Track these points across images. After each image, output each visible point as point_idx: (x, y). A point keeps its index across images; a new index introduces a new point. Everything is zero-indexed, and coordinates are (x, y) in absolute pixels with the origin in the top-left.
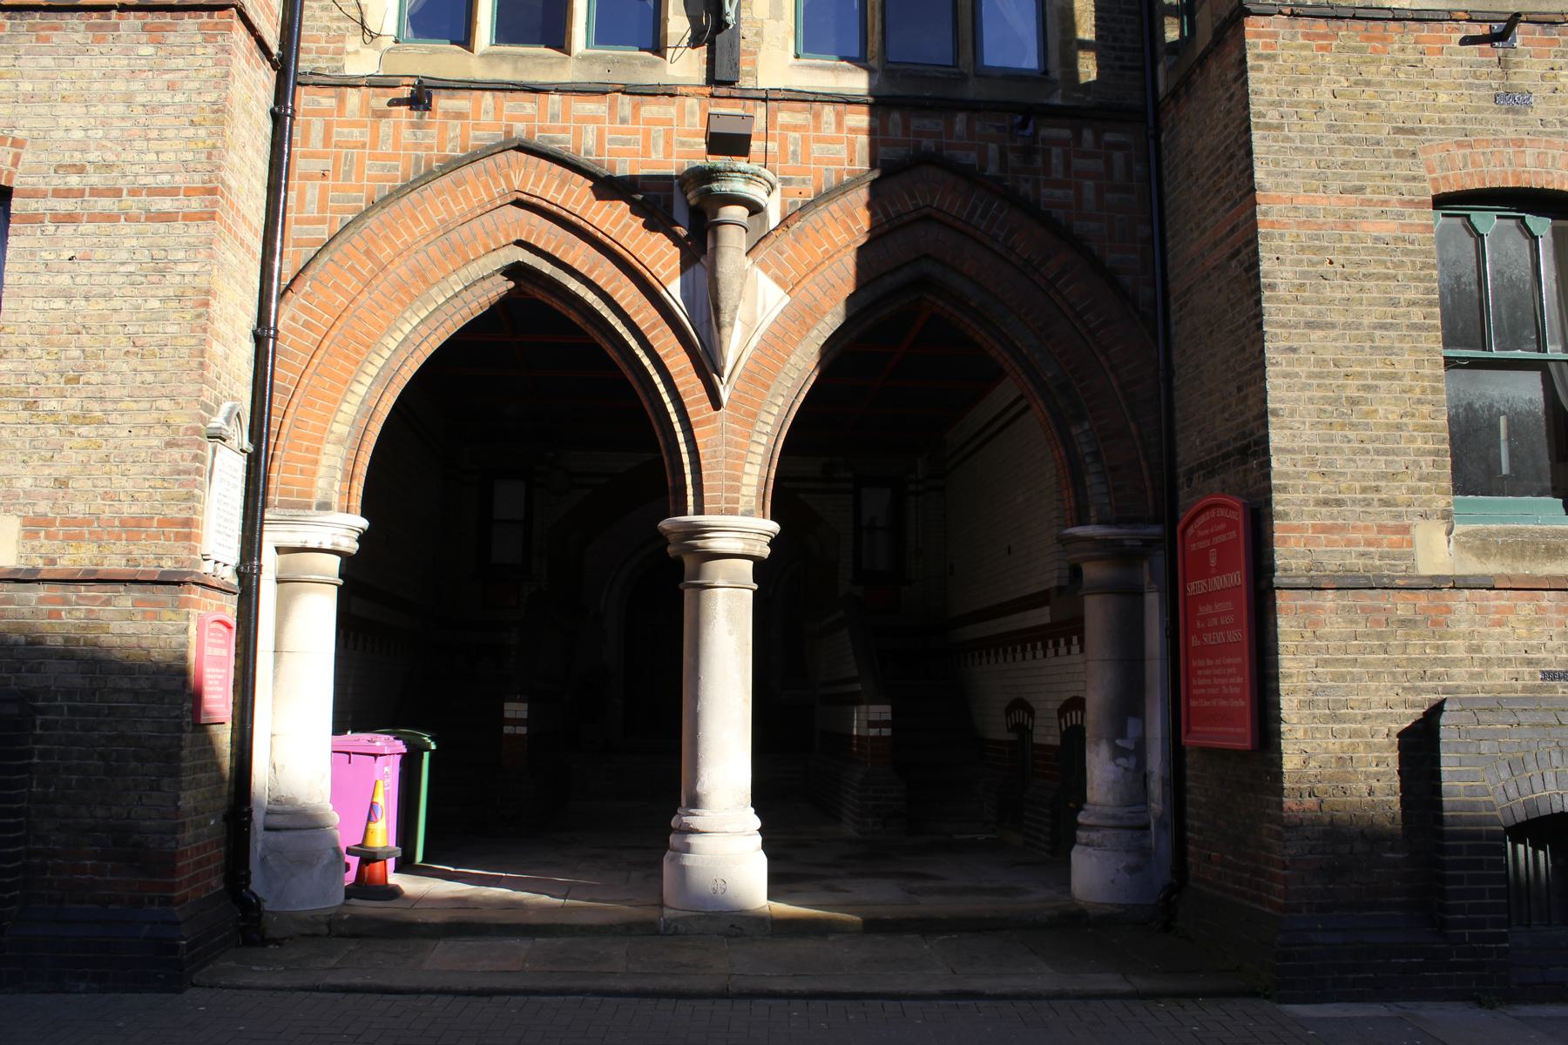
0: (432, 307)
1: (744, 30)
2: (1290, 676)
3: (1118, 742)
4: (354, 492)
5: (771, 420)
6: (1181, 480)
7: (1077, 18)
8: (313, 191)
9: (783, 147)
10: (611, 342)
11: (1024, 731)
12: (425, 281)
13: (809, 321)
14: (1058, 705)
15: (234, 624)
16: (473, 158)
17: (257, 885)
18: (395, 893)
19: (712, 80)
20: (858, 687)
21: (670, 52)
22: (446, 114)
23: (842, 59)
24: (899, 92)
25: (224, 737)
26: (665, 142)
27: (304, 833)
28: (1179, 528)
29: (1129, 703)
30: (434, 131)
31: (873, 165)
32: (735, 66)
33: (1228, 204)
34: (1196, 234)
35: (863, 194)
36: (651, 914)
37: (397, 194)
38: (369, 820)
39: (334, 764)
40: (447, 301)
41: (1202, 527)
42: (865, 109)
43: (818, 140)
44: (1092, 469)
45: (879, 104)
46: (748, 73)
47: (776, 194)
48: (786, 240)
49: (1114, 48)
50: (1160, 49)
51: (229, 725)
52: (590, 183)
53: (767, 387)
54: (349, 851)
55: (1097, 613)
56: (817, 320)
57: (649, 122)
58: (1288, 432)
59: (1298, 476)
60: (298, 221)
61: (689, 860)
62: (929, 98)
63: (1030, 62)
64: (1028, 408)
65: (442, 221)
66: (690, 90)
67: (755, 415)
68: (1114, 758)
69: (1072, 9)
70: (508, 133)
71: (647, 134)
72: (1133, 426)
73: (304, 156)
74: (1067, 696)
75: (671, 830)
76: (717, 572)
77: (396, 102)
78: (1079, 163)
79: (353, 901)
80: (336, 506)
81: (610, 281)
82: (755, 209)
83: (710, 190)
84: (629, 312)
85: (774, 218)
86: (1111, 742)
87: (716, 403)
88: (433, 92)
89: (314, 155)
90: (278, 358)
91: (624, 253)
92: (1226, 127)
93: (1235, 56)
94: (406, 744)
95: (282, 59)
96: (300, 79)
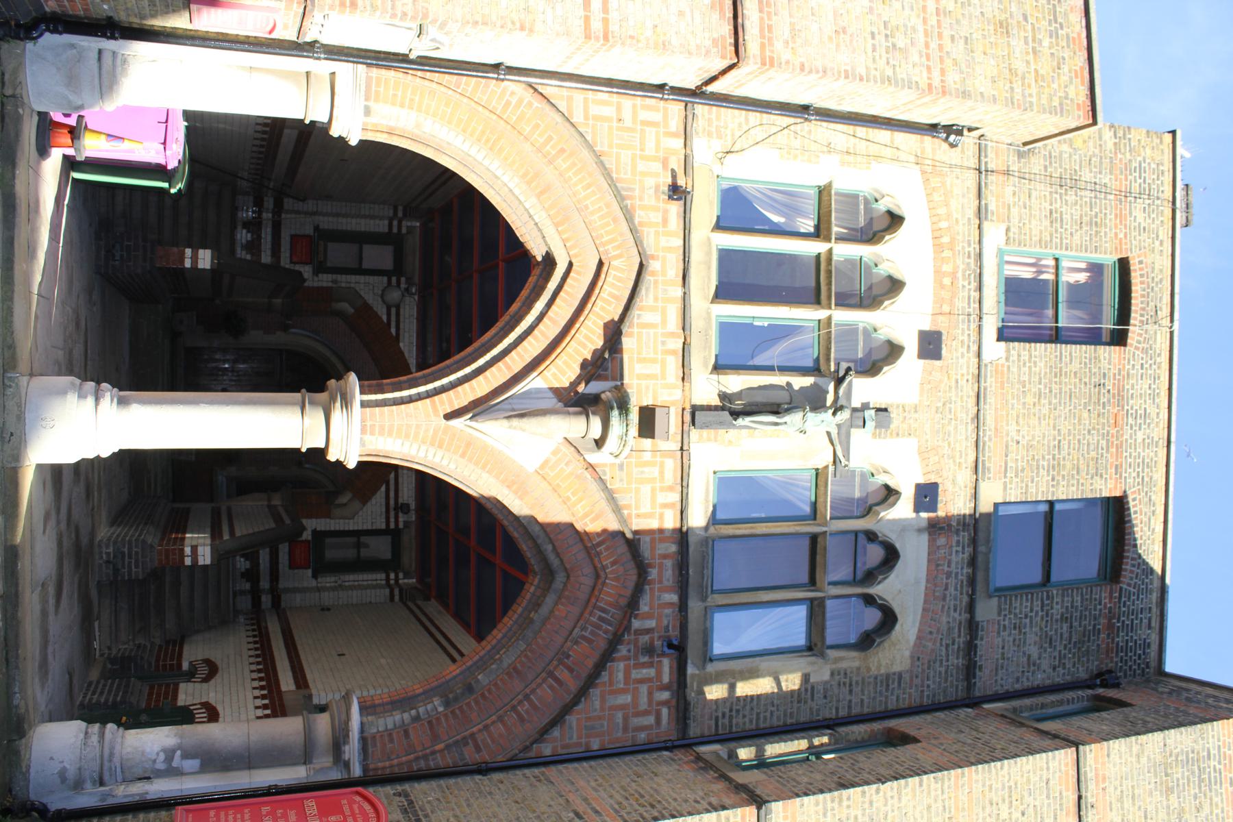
0: (522, 198)
1: (732, 432)
3: (179, 753)
4: (379, 135)
5: (437, 460)
6: (399, 788)
7: (752, 681)
8: (609, 111)
9: (646, 464)
10: (496, 334)
11: (190, 675)
12: (542, 193)
13: (515, 487)
14: (213, 702)
15: (273, 36)
16: (633, 230)
17: (49, 39)
18: (43, 152)
19: (695, 409)
20: (226, 537)
21: (715, 377)
22: (666, 212)
23: (715, 507)
24: (691, 549)
25: (179, 22)
26: (648, 374)
27: (97, 81)
28: (360, 789)
29: (214, 760)
30: (653, 202)
31: (636, 533)
32: (706, 426)
33: (617, 807)
34: (593, 784)
35: (614, 526)
36: (23, 365)
37: (607, 174)
38: (109, 135)
39: (157, 110)
40: (526, 210)
41: (361, 807)
42: (678, 525)
43: (653, 490)
44: (406, 716)
45: (682, 536)
46: (701, 436)
47: (612, 460)
48: (577, 467)
49: (731, 710)
50: (732, 745)
51: (190, 27)
52: (616, 319)
53: (463, 455)
54: (81, 117)
55: (288, 728)
56: (516, 493)
57: (663, 363)
60: (586, 100)
61: (72, 398)
62: (687, 573)
63: (718, 648)
64: (454, 660)
65: (587, 207)
66: (687, 393)
67: (440, 447)
68: (164, 750)
69: (758, 677)
70: (653, 257)
71: (654, 361)
72: (442, 746)
73: (634, 106)
74: (220, 709)
75: (98, 383)
76: (315, 418)
77: (674, 176)
78: (644, 689)
79: (36, 118)
80: (368, 120)
81: (543, 334)
82: (599, 443)
83: (612, 408)
84: (519, 348)
85: (594, 457)
86: (180, 747)
87: (448, 417)
88: (682, 202)
89: (635, 113)
90: (484, 81)
91: (563, 345)
92: (675, 800)
93: (727, 801)
94: (175, 170)
95: (703, 93)
96: (689, 105)
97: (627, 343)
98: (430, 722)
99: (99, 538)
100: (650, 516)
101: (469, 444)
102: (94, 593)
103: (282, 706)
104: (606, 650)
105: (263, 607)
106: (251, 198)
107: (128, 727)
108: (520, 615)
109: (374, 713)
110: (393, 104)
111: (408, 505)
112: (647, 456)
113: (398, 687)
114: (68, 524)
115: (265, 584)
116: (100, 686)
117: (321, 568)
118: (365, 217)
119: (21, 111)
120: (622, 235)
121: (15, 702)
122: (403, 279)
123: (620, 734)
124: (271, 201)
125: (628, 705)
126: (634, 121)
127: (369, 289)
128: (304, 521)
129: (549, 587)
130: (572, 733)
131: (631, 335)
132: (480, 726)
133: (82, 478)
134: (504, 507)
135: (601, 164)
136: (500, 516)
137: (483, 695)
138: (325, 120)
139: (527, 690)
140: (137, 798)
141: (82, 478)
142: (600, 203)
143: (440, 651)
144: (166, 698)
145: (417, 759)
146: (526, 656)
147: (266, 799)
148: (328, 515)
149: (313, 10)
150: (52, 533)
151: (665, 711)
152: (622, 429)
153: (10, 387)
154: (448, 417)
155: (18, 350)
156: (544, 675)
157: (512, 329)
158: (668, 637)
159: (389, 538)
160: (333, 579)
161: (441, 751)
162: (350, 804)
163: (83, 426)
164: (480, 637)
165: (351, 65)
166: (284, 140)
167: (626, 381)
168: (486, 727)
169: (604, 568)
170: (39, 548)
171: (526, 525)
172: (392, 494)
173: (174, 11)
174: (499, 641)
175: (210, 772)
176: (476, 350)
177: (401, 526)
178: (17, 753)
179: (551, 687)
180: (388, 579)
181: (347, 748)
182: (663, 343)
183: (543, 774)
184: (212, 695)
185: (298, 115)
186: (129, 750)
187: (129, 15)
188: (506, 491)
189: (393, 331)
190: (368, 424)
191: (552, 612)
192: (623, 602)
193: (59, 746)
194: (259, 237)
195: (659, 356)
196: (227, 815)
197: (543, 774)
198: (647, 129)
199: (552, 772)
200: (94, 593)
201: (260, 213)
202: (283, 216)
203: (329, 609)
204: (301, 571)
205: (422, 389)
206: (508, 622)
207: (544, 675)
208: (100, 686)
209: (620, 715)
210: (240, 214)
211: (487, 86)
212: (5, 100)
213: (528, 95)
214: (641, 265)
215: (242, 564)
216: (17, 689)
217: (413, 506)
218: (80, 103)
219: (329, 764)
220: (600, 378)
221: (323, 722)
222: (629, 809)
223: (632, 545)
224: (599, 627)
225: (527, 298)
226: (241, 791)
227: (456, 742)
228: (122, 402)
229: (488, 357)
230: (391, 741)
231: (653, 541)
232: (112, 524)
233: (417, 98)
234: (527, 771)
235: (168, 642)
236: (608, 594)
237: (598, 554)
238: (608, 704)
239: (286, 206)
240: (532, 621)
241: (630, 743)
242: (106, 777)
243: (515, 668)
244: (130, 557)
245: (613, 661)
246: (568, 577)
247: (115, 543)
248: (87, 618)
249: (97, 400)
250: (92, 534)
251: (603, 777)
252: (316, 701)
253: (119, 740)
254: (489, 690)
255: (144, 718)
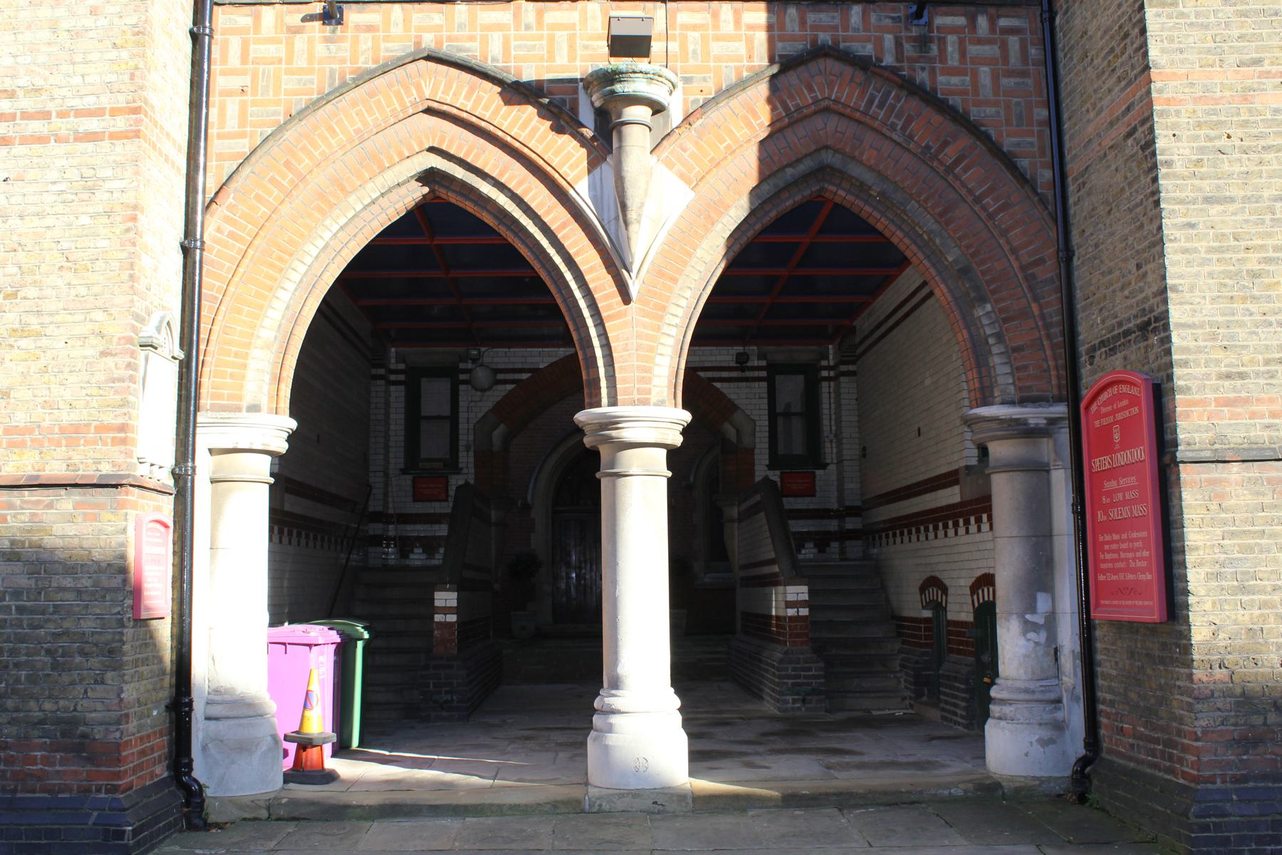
0: (350, 214)
2: (1197, 548)
3: (1028, 617)
4: (282, 394)
5: (680, 312)
6: (1084, 358)
8: (232, 106)
9: (683, 46)
10: (523, 242)
11: (939, 608)
12: (343, 189)
13: (713, 215)
14: (970, 582)
16: (385, 70)
17: (199, 772)
18: (331, 777)
20: (776, 569)
22: (358, 28)
25: (164, 631)
27: (242, 721)
28: (1082, 405)
29: (1039, 576)
30: (346, 45)
31: (772, 61)
33: (1123, 83)
34: (1092, 115)
35: (762, 89)
36: (575, 792)
37: (314, 106)
38: (305, 707)
40: (365, 208)
41: (1105, 404)
44: (995, 350)
47: (678, 93)
48: (687, 138)
51: (168, 620)
52: (499, 89)
53: (675, 281)
54: (287, 738)
56: (721, 214)
57: (554, 27)
58: (1188, 307)
59: (1199, 350)
60: (220, 136)
61: (612, 739)
64: (931, 294)
65: (358, 131)
67: (664, 308)
68: (1024, 633)
70: (418, 44)
71: (551, 39)
73: (223, 73)
74: (979, 573)
75: (594, 711)
76: (631, 460)
77: (309, 18)
78: (973, 50)
79: (291, 785)
80: (265, 407)
81: (520, 184)
82: (657, 108)
83: (613, 92)
85: (676, 114)
86: (1021, 616)
87: (626, 299)
90: (205, 267)
94: (340, 633)
97: (529, 74)
98: (1005, 320)
99: (777, 712)
100: (750, 41)
101: (661, 274)
102: (840, 716)
103: (977, 501)
104: (922, 99)
105: (859, 526)
106: (371, 549)
107: (996, 674)
108: (875, 208)
109: (991, 388)
110: (243, 377)
111: (738, 355)
112: (674, 46)
113: (960, 362)
114: (760, 743)
115: (833, 525)
116: (948, 707)
117: (814, 458)
118: (387, 414)
119: (284, 801)
120: (390, 85)
121: (960, 793)
122: (462, 366)
123: (1030, 81)
124: (372, 526)
125: (993, 71)
126: (243, 73)
127: (476, 407)
128: (758, 479)
129: (840, 172)
130: (1025, 143)
131: (519, 70)
132: (1012, 258)
133: (705, 729)
134: (737, 228)
135: (302, 114)
136: (750, 233)
137: (973, 255)
138: (268, 459)
139: (970, 199)
140: (1078, 662)
141: (705, 729)
142: (353, 113)
143: (916, 313)
144: (963, 634)
145: (1049, 337)
146: (926, 201)
147: (1088, 516)
148: (751, 451)
149: (134, 476)
150: (770, 760)
151: (1003, 22)
152: (640, 79)
153: (600, 805)
154: (626, 299)
155: (559, 798)
156: (950, 178)
157: (516, 221)
158: (907, 17)
159: (778, 378)
160: (828, 445)
161: (1041, 307)
162: (1099, 416)
163: (644, 723)
164: (904, 262)
165: (198, 430)
166: (298, 510)
167: (577, 75)
168: (1014, 251)
169: (816, 101)
170: (784, 773)
171: (761, 200)
172: (725, 374)
173: (151, 637)
174: (907, 235)
175: (1052, 579)
176: (543, 266)
177: (763, 363)
178: (1018, 790)
179: (965, 170)
180: (828, 379)
181: (1032, 421)
182: (528, 27)
183: (1075, 179)
184: (962, 582)
185: (265, 490)
186: (1022, 671)
187: (162, 688)
188: (719, 227)
189: (525, 376)
190: (636, 397)
191: (871, 168)
192: (860, 76)
193: (1011, 748)
194: (418, 538)
195: (545, 32)
196: (1105, 561)
197: (1075, 179)
198: (252, 55)
199: (1073, 168)
200: (840, 716)
201: (389, 539)
202: (391, 511)
203: (864, 449)
204: (817, 483)
205: (593, 332)
206: (882, 223)
207: (950, 178)
208: (948, 707)
209: (1005, 81)
210: (392, 563)
211: (212, 263)
212: (273, 817)
213: (219, 211)
214: (429, 58)
215: (809, 552)
216: (946, 792)
217: (740, 349)
218: (269, 739)
219: (1051, 442)
220: (574, 109)
221: (1000, 450)
222: (1127, 68)
223: (788, 65)
224: (892, 107)
225: (476, 203)
226: (1077, 545)
227: (1031, 289)
228: (616, 684)
229: (551, 251)
230: (1025, 368)
231: (782, 39)
232: (761, 698)
233: (234, 349)
234: (1071, 200)
235: (899, 635)
236: (850, 96)
237: (798, 109)
238: (991, 97)
239: (380, 509)
240: (882, 194)
241: (1042, 69)
242: (1052, 696)
243: (941, 215)
244: (799, 677)
245: (935, 90)
246: (827, 147)
247: (781, 693)
248: (868, 723)
249: (614, 712)
250: (772, 718)
251: (1084, 102)
252: (974, 462)
253: (1010, 683)
254: (968, 247)
255: (986, 658)
